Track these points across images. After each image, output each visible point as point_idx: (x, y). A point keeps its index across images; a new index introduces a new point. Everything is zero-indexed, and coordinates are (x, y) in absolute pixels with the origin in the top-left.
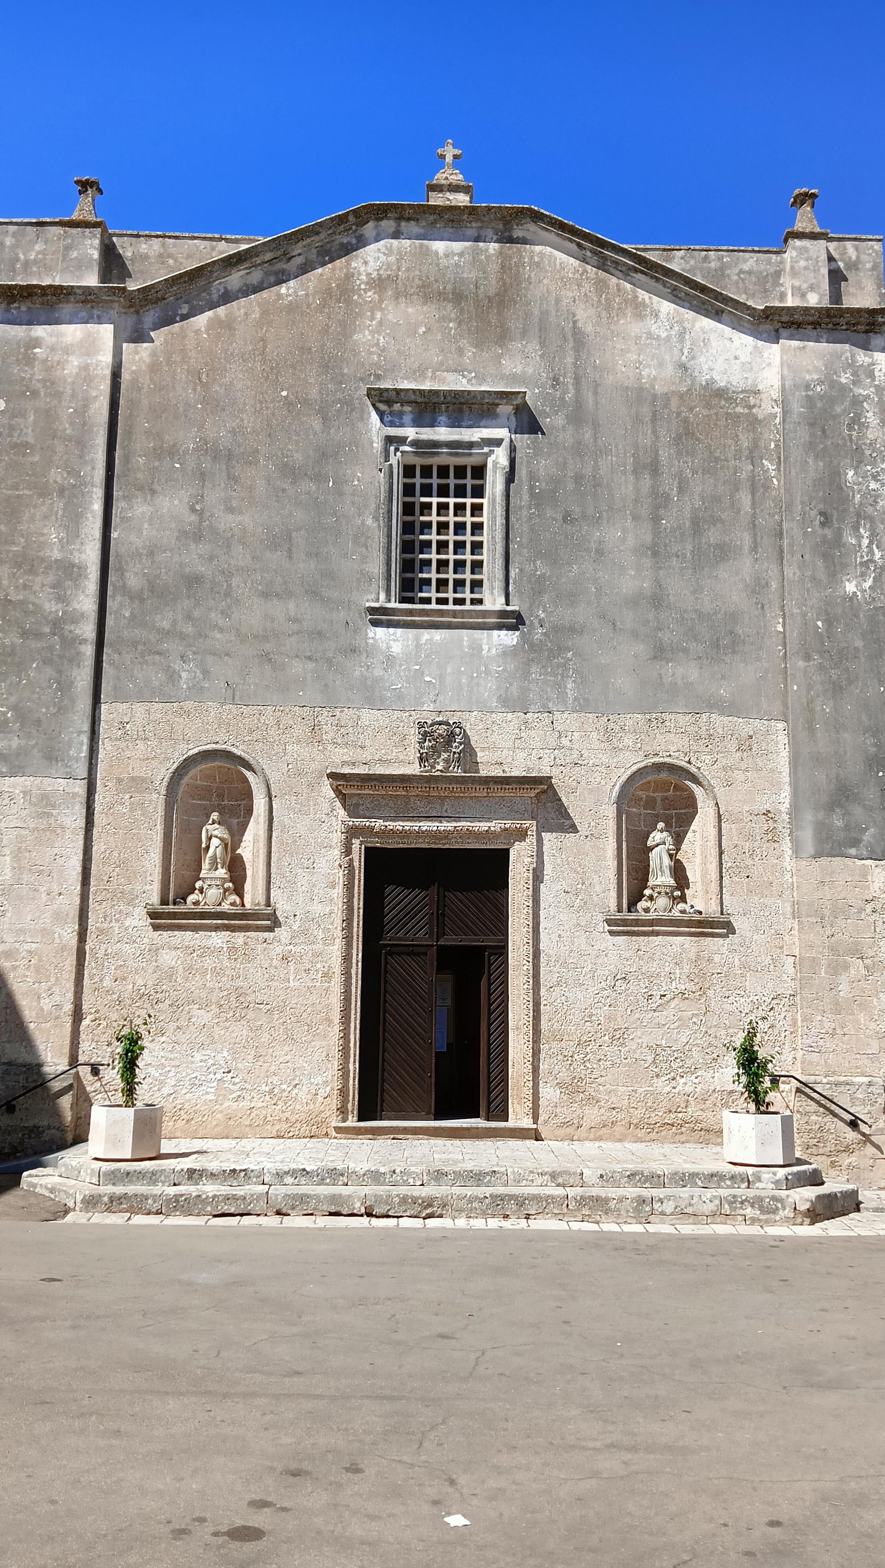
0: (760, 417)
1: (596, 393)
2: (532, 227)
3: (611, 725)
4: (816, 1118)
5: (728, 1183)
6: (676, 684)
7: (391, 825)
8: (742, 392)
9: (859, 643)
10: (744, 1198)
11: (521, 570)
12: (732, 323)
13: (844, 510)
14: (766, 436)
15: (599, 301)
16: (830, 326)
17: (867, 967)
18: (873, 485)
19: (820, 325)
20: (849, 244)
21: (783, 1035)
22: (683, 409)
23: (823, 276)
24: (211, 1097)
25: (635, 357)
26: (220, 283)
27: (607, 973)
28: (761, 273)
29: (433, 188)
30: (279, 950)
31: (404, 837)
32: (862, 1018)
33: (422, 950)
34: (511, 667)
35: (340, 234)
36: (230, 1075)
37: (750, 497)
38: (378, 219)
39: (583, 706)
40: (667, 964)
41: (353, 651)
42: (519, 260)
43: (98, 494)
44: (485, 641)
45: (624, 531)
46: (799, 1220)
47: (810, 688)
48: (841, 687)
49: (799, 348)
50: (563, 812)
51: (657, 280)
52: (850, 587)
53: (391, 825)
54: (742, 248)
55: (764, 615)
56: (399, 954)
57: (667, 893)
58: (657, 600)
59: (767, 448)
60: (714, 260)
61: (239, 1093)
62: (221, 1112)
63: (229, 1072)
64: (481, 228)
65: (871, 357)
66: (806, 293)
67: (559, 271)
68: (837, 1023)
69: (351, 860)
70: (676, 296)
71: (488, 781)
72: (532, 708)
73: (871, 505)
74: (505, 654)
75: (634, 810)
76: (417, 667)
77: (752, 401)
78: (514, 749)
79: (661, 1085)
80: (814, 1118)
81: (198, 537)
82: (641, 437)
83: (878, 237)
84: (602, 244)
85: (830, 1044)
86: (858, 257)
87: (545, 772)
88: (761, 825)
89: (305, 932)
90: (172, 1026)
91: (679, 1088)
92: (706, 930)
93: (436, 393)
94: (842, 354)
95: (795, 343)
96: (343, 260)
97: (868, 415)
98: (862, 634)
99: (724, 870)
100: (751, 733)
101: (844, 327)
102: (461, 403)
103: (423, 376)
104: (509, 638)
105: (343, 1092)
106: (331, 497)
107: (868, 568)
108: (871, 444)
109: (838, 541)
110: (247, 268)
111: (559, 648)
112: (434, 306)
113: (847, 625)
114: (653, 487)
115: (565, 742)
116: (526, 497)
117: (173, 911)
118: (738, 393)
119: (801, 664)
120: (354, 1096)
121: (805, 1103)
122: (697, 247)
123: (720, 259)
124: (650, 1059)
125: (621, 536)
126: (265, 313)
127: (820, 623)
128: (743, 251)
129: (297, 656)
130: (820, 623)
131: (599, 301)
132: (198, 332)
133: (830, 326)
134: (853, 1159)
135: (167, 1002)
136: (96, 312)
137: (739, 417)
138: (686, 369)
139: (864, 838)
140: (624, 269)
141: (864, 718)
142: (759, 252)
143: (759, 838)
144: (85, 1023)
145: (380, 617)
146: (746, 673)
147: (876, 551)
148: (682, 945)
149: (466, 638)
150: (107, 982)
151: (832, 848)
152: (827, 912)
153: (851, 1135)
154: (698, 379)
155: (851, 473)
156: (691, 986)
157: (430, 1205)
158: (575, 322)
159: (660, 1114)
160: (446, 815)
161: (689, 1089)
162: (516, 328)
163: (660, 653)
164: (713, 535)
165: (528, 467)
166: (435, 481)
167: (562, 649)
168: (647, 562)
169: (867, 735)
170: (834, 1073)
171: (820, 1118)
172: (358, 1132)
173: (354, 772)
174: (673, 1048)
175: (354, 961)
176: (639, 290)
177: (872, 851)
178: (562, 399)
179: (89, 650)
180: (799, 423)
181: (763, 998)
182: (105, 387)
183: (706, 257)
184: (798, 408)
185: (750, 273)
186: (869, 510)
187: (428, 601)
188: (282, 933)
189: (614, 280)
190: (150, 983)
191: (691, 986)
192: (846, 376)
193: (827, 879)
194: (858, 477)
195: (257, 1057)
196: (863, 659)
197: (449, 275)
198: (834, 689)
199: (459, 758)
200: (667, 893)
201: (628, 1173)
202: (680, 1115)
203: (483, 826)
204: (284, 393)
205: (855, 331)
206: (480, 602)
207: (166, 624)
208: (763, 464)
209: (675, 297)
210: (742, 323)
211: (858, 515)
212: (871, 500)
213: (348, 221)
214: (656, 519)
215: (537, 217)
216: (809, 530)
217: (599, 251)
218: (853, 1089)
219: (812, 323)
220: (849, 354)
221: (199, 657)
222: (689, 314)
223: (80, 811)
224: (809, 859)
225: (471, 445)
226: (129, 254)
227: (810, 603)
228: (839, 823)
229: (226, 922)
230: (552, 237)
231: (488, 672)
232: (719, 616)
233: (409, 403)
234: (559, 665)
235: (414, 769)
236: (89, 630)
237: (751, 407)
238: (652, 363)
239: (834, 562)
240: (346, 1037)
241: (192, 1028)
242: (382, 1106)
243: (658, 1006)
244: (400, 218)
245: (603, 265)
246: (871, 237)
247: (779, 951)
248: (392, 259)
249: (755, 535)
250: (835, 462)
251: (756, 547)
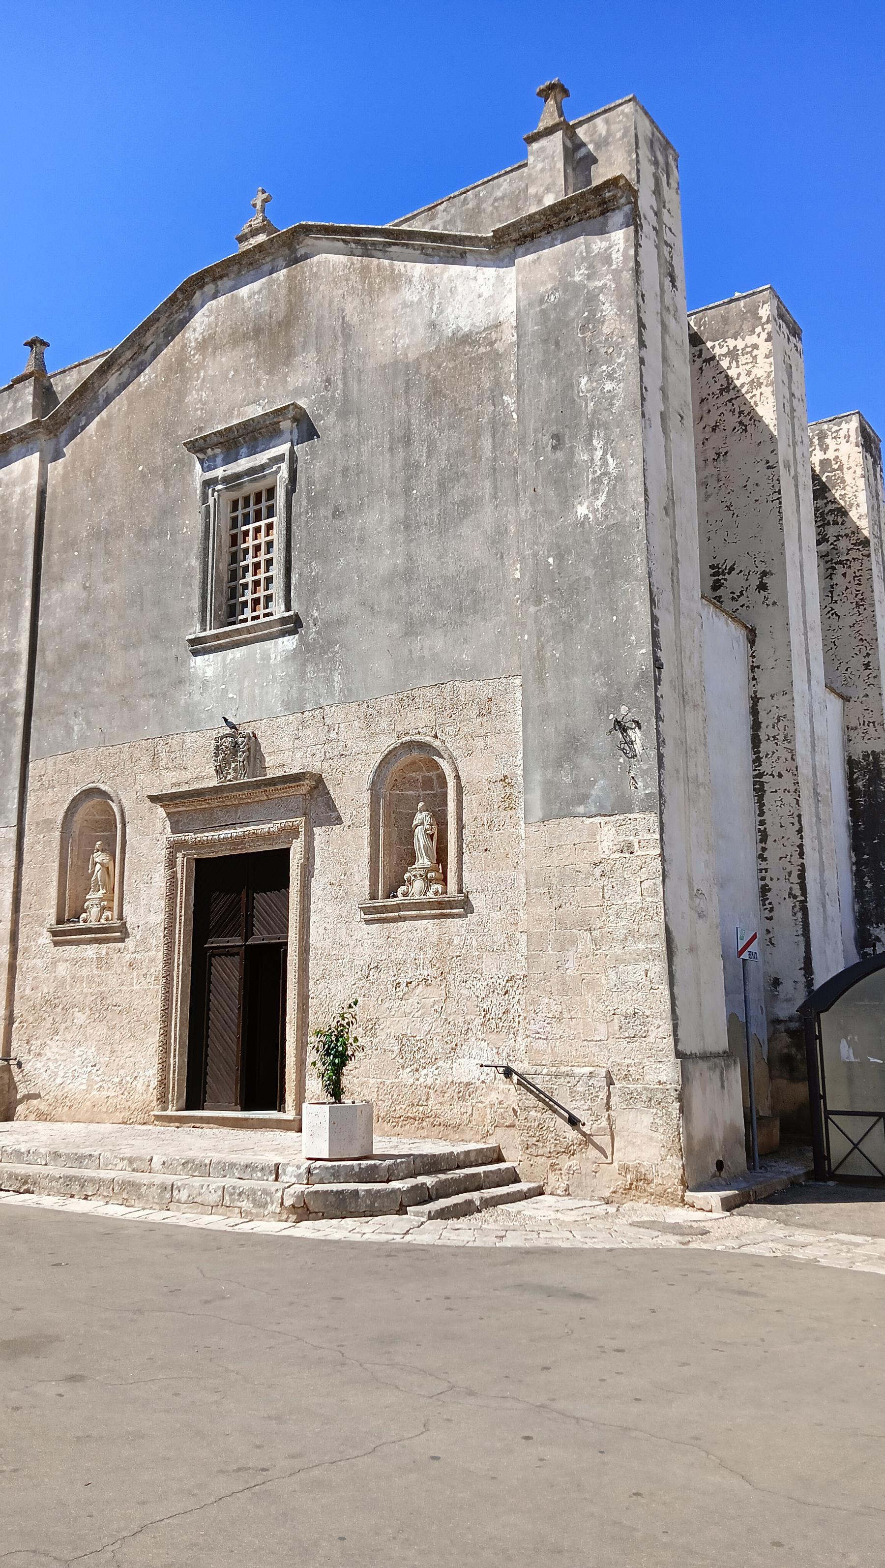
0: (501, 351)
1: (360, 381)
2: (309, 241)
3: (370, 711)
4: (535, 1114)
5: (259, 1174)
6: (423, 657)
7: (201, 836)
8: (484, 331)
9: (589, 572)
10: (241, 1189)
11: (300, 575)
12: (477, 260)
13: (577, 425)
14: (506, 370)
15: (363, 287)
16: (562, 223)
17: (595, 941)
18: (608, 386)
19: (552, 227)
20: (599, 121)
21: (517, 1021)
22: (432, 369)
23: (559, 171)
24: (84, 1087)
25: (392, 331)
26: (103, 390)
27: (362, 963)
28: (513, 192)
29: (242, 239)
30: (127, 958)
31: (211, 847)
32: (589, 999)
33: (235, 950)
34: (291, 671)
35: (176, 312)
36: (96, 1068)
37: (490, 440)
38: (201, 287)
39: (348, 696)
40: (413, 949)
41: (180, 682)
42: (302, 277)
43: (28, 592)
44: (272, 650)
45: (382, 512)
46: (285, 1217)
47: (540, 633)
48: (571, 626)
49: (534, 262)
50: (330, 805)
51: (407, 245)
52: (582, 510)
53: (201, 836)
54: (496, 175)
55: (503, 564)
56: (220, 955)
57: (421, 876)
58: (408, 575)
59: (507, 382)
60: (472, 199)
61: (100, 1084)
62: (89, 1100)
63: (95, 1065)
64: (274, 259)
65: (608, 240)
66: (543, 197)
67: (332, 274)
68: (564, 1005)
69: (175, 873)
70: (427, 255)
71: (273, 782)
72: (308, 707)
73: (606, 410)
74: (287, 659)
75: (411, 792)
76: (223, 687)
77: (494, 336)
78: (293, 750)
79: (406, 1077)
80: (533, 1113)
81: (86, 609)
82: (396, 411)
83: (627, 98)
84: (357, 232)
85: (557, 1030)
86: (608, 131)
87: (316, 766)
88: (499, 792)
89: (144, 940)
90: (63, 1025)
91: (422, 1080)
92: (445, 911)
93: (229, 429)
94: (576, 249)
95: (530, 258)
96: (180, 335)
97: (604, 307)
98: (592, 561)
99: (465, 846)
100: (490, 695)
101: (576, 219)
102: (252, 432)
103: (231, 416)
104: (289, 643)
105: (163, 1083)
106: (168, 549)
107: (601, 483)
108: (607, 340)
109: (570, 463)
110: (117, 371)
111: (329, 643)
112: (240, 349)
113: (578, 554)
114: (405, 459)
115: (333, 735)
116: (304, 503)
117: (68, 928)
118: (481, 333)
119: (532, 609)
120: (174, 1087)
121: (524, 1097)
122: (456, 193)
123: (477, 195)
124: (396, 1049)
125: (377, 518)
126: (130, 403)
127: (551, 560)
128: (497, 177)
129: (144, 696)
130: (551, 560)
131: (363, 287)
132: (90, 437)
133: (562, 223)
134: (574, 1162)
135: (61, 1007)
136: (30, 446)
137: (482, 358)
138: (434, 326)
139: (593, 792)
140: (381, 247)
141: (594, 656)
142: (512, 171)
143: (496, 807)
144: (16, 1025)
145: (199, 646)
146: (486, 630)
147: (610, 460)
148: (425, 928)
149: (258, 651)
150: (28, 992)
151: (560, 809)
152: (555, 881)
153: (571, 1134)
154: (445, 333)
155: (584, 381)
156: (433, 972)
157: (26, 1183)
158: (343, 318)
159: (404, 1107)
160: (239, 821)
161: (430, 1081)
162: (299, 342)
163: (411, 629)
164: (457, 493)
165: (306, 473)
166: (252, 509)
167: (331, 643)
168: (400, 537)
169: (597, 675)
170: (561, 1062)
171: (539, 1114)
172: (182, 1120)
173: (181, 790)
174: (417, 1038)
175: (176, 965)
176: (395, 262)
177: (602, 806)
178: (333, 397)
179: (20, 721)
180: (533, 343)
181: (499, 981)
182: (33, 505)
183: (465, 199)
184: (532, 327)
185: (502, 198)
186: (604, 416)
187: (245, 620)
188: (130, 943)
189: (375, 261)
190: (51, 991)
191: (433, 972)
192: (581, 272)
193: (555, 843)
194: (592, 383)
195: (113, 1052)
196: (594, 589)
197: (251, 314)
198: (564, 630)
199: (244, 766)
200: (421, 876)
201: (183, 1161)
202: (421, 1108)
203: (264, 828)
204: (140, 468)
205: (590, 218)
206: (270, 614)
207: (66, 689)
208: (503, 401)
209: (427, 256)
210: (483, 256)
211: (591, 426)
212: (606, 404)
213: (178, 299)
214: (407, 491)
215: (307, 230)
216: (542, 458)
217: (360, 240)
218: (573, 1081)
219: (544, 229)
220: (583, 247)
221: (84, 711)
222: (437, 268)
223: (12, 852)
224: (538, 824)
225: (263, 467)
226: (59, 389)
227: (541, 540)
228: (568, 780)
229: (93, 936)
230: (324, 243)
231: (274, 679)
232: (462, 576)
233: (216, 445)
234: (330, 660)
235: (214, 783)
236: (20, 705)
237: (491, 344)
238: (406, 332)
239: (566, 487)
240: (166, 1034)
241: (74, 1027)
242: (204, 1097)
243: (404, 994)
244: (215, 280)
245: (367, 251)
246: (620, 101)
247: (514, 927)
248: (212, 318)
249: (495, 479)
250: (568, 374)
251: (496, 493)
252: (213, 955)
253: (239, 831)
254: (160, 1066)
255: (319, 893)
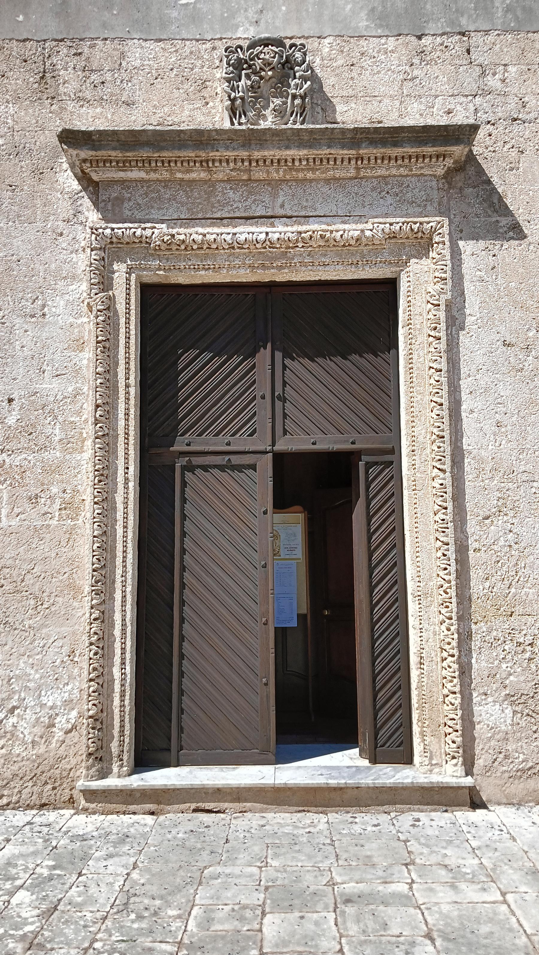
50: (495, 203)
56: (205, 468)
69: (112, 299)
105: (100, 722)
115: (493, 82)
120: (122, 726)
160: (281, 212)
252: (190, 468)
253: (280, 231)
254: (94, 686)
255: (479, 360)
